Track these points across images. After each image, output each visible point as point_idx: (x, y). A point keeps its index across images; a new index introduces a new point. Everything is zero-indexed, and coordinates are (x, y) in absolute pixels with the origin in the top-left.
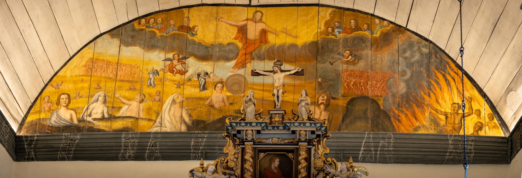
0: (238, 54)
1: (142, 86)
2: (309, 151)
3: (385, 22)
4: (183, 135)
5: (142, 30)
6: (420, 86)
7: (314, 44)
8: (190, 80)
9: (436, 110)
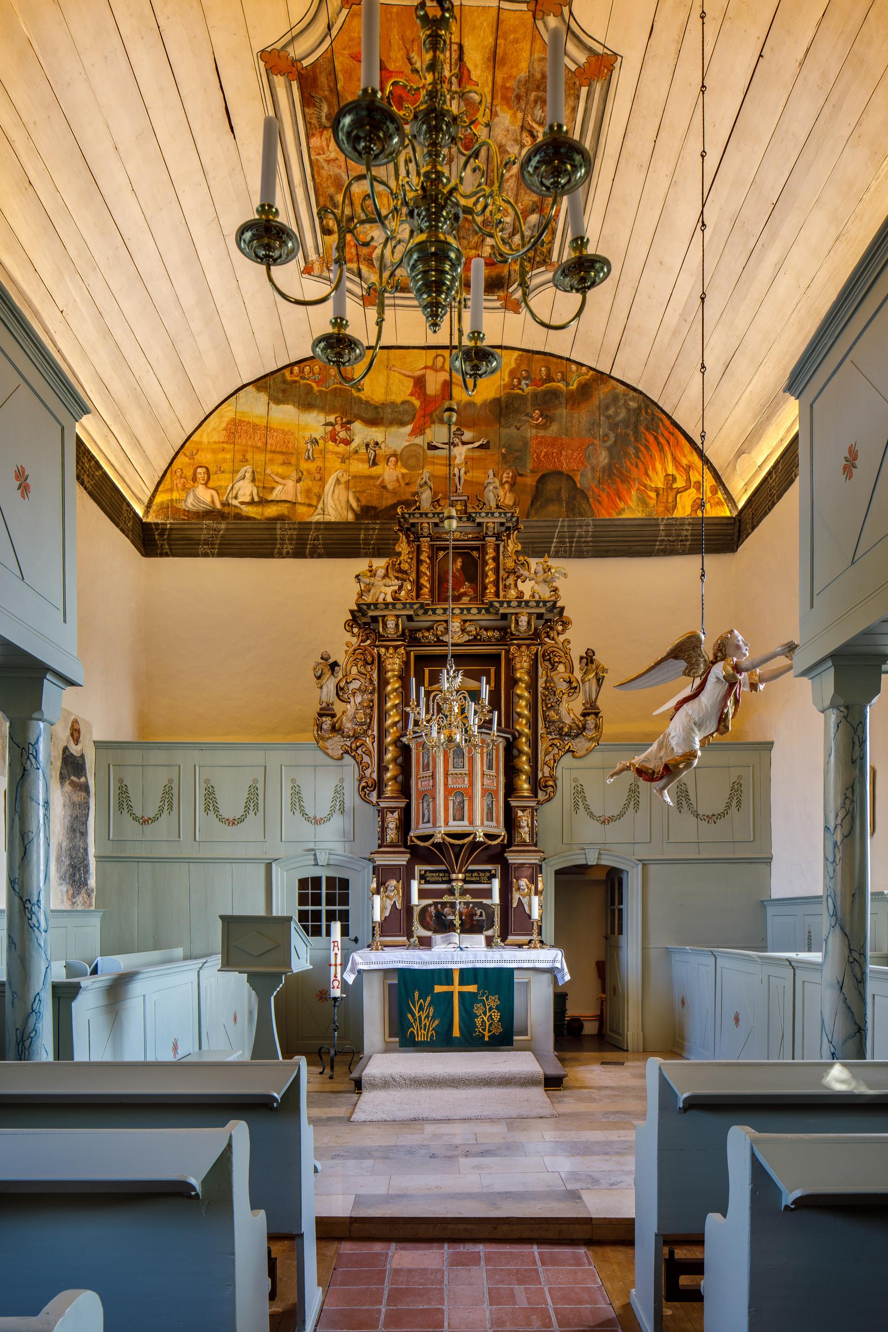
0: (414, 417)
1: (298, 460)
3: (584, 368)
4: (351, 526)
5: (295, 382)
6: (626, 454)
7: (497, 401)
8: (356, 452)
9: (645, 486)
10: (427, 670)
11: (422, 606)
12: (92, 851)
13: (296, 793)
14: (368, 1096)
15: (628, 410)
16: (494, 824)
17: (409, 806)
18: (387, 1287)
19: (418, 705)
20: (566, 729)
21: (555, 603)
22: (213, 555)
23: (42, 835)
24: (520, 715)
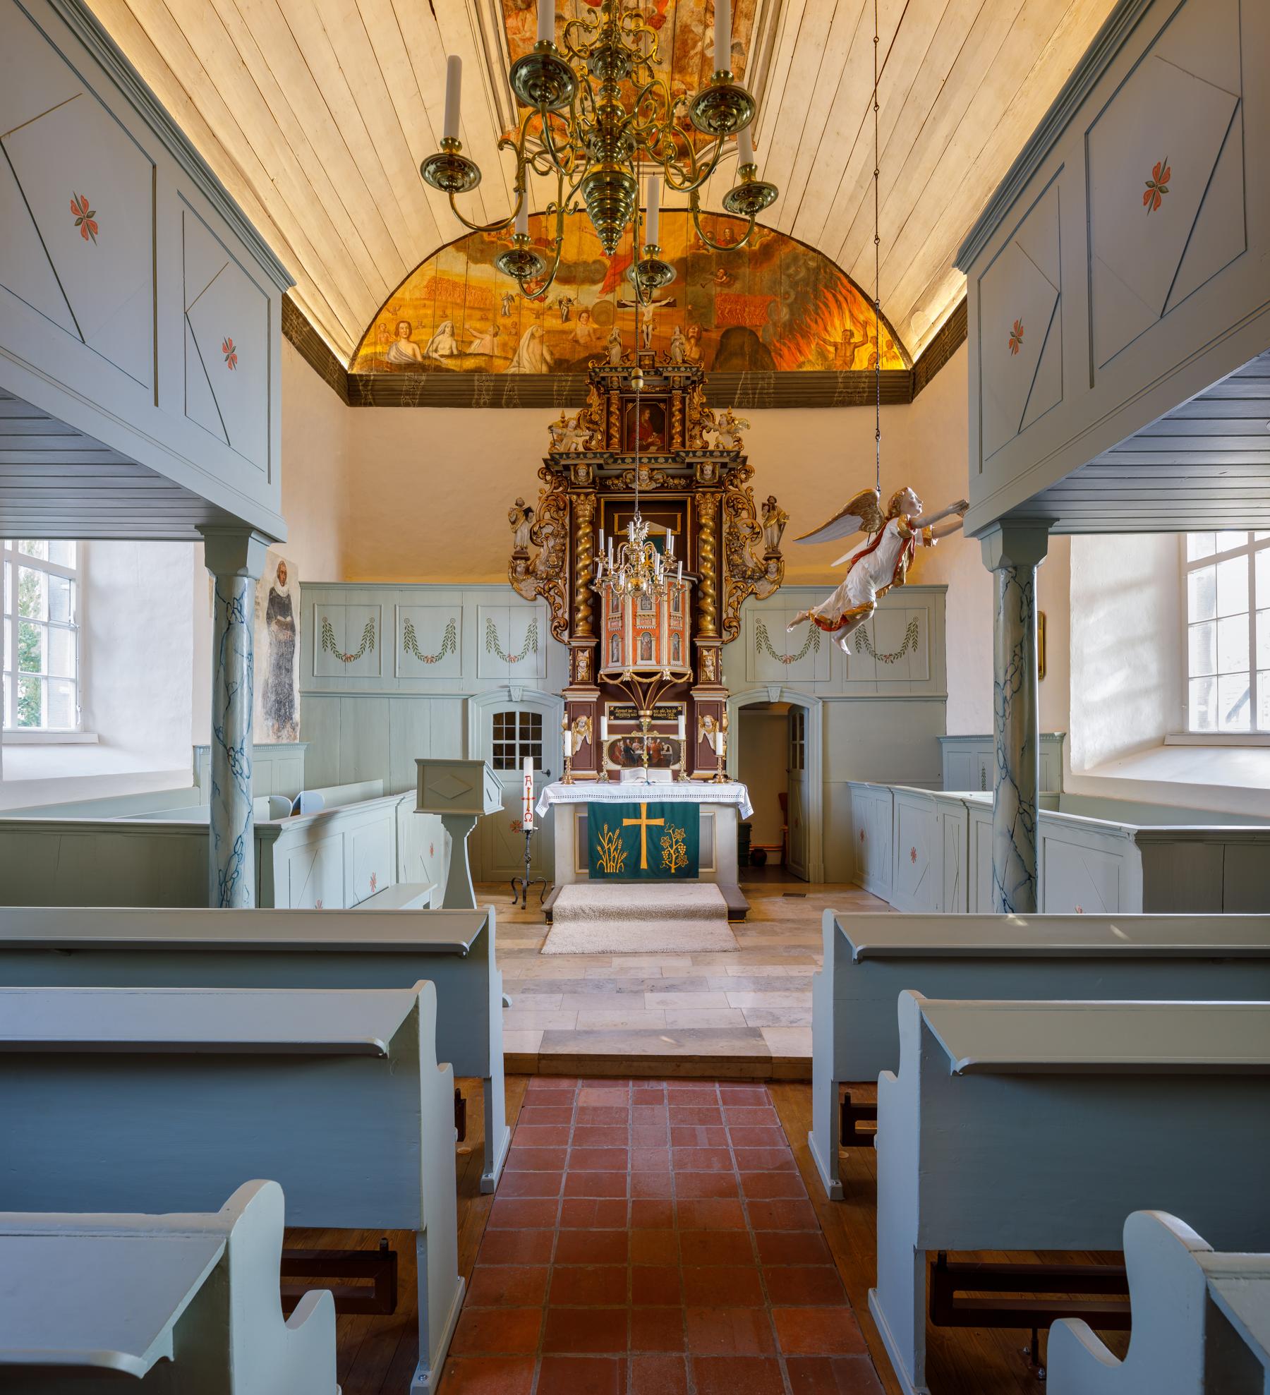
1: (495, 315)
2: (683, 401)
6: (806, 311)
8: (550, 308)
10: (616, 516)
11: (612, 455)
12: (297, 686)
13: (492, 632)
14: (558, 927)
15: (808, 269)
16: (680, 663)
17: (599, 645)
18: (573, 1125)
19: (606, 555)
20: (749, 573)
21: (738, 453)
22: (414, 405)
23: (245, 685)
24: (705, 559)
